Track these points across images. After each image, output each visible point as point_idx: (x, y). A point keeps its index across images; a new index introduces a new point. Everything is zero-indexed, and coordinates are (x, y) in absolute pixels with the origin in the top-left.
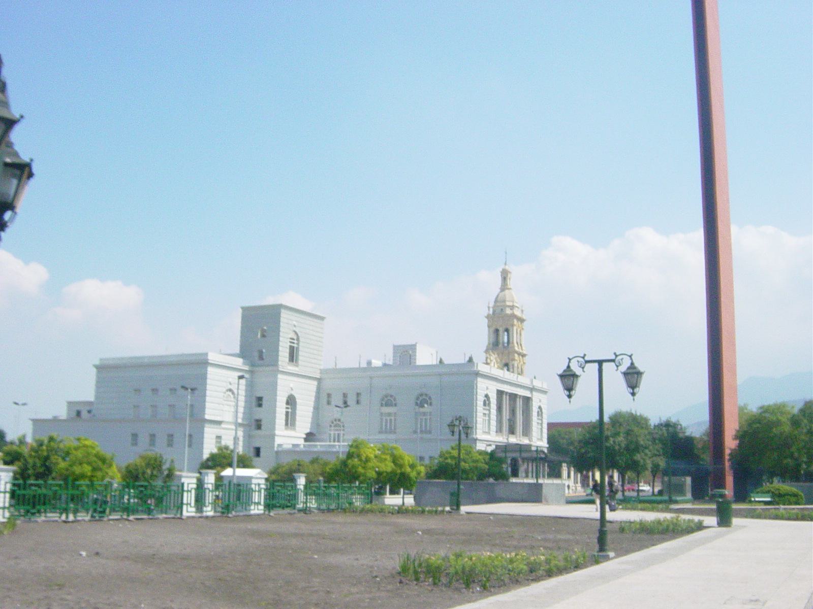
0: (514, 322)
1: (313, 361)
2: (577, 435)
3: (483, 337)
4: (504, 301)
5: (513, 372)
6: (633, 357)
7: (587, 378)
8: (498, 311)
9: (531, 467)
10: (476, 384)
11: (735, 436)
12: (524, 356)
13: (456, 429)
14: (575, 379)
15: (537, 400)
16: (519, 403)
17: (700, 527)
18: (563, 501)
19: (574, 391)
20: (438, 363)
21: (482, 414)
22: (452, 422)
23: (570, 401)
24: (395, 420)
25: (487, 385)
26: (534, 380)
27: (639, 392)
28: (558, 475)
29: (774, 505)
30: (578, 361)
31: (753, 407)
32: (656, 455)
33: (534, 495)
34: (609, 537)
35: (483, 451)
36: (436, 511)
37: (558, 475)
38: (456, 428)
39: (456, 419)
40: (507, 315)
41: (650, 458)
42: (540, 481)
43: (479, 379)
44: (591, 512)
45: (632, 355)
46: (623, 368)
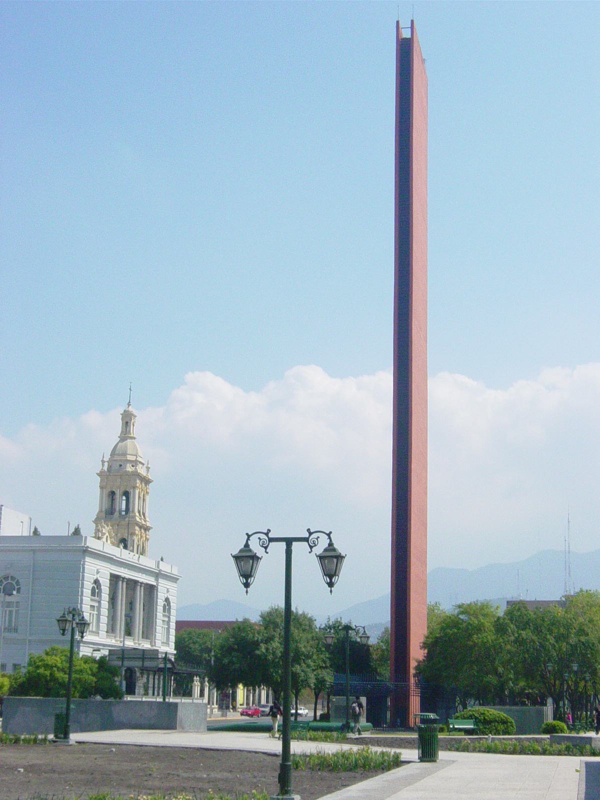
0: (136, 483)
2: (216, 639)
3: (92, 501)
4: (125, 454)
5: (133, 551)
6: (331, 535)
7: (271, 562)
8: (116, 466)
9: (159, 681)
10: (84, 564)
11: (424, 643)
12: (147, 529)
13: (68, 627)
14: (255, 562)
15: (164, 589)
16: (140, 594)
17: (397, 762)
18: (204, 727)
19: (252, 578)
20: (31, 534)
21: (89, 607)
22: (64, 616)
23: (247, 592)
24: (17, 612)
25: (98, 567)
26: (161, 562)
27: (337, 584)
28: (188, 693)
29: (477, 734)
30: (259, 538)
31: (447, 607)
32: (321, 667)
33: (166, 719)
34: (294, 774)
35: (90, 657)
36: (35, 740)
37: (188, 693)
38: (68, 624)
39: (70, 612)
40: (127, 473)
41: (313, 670)
42: (171, 700)
43: (87, 559)
44: (271, 744)
45: (247, 534)
46: (319, 549)
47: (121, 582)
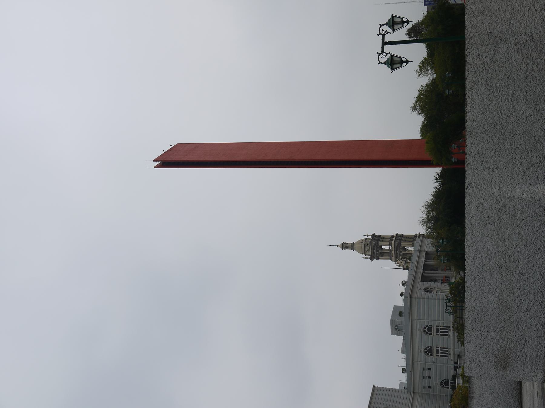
1: (402, 397)
46: (390, 30)
47: (426, 274)
